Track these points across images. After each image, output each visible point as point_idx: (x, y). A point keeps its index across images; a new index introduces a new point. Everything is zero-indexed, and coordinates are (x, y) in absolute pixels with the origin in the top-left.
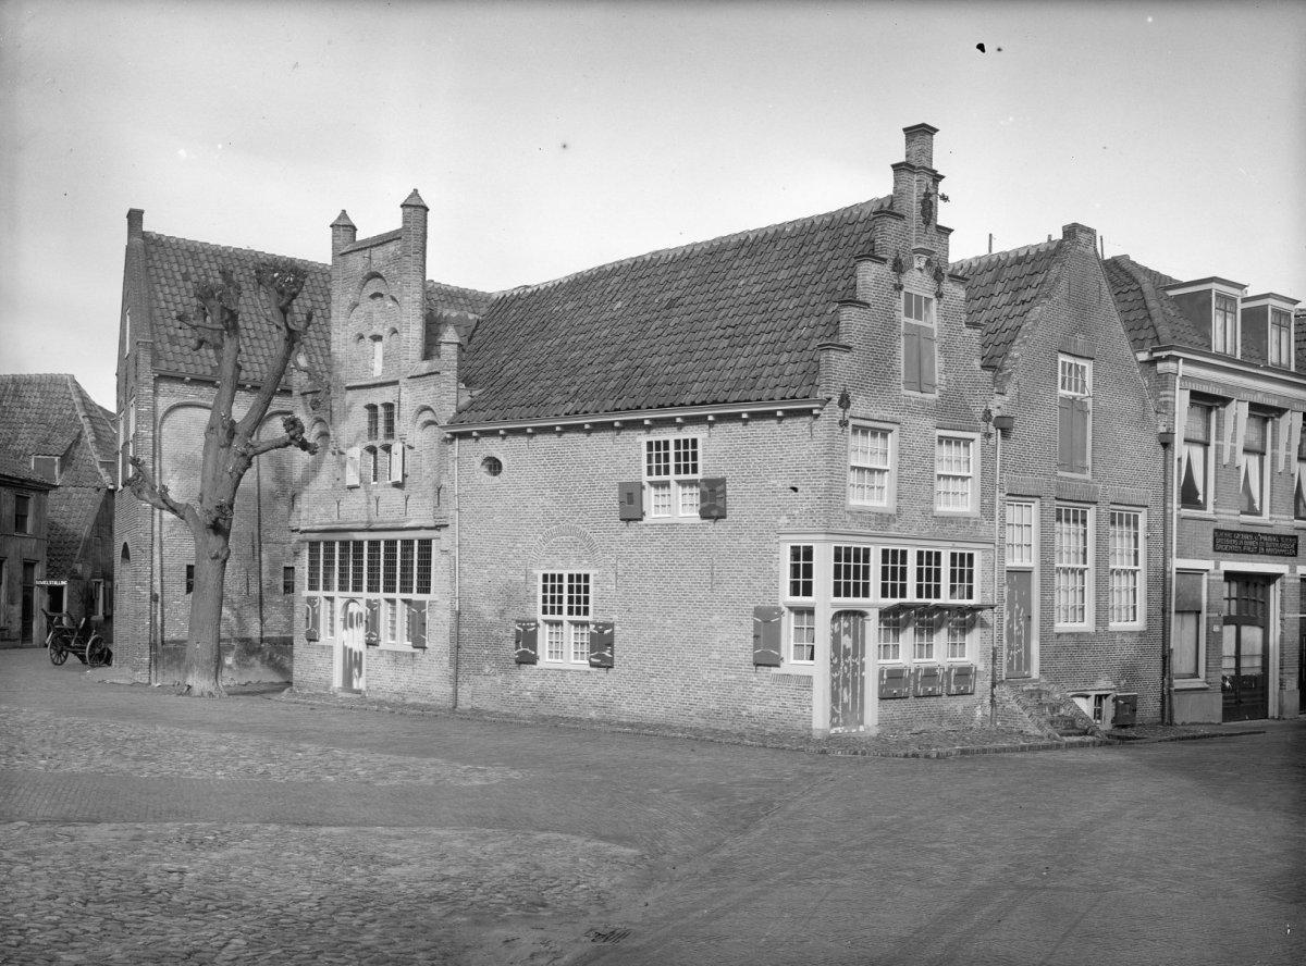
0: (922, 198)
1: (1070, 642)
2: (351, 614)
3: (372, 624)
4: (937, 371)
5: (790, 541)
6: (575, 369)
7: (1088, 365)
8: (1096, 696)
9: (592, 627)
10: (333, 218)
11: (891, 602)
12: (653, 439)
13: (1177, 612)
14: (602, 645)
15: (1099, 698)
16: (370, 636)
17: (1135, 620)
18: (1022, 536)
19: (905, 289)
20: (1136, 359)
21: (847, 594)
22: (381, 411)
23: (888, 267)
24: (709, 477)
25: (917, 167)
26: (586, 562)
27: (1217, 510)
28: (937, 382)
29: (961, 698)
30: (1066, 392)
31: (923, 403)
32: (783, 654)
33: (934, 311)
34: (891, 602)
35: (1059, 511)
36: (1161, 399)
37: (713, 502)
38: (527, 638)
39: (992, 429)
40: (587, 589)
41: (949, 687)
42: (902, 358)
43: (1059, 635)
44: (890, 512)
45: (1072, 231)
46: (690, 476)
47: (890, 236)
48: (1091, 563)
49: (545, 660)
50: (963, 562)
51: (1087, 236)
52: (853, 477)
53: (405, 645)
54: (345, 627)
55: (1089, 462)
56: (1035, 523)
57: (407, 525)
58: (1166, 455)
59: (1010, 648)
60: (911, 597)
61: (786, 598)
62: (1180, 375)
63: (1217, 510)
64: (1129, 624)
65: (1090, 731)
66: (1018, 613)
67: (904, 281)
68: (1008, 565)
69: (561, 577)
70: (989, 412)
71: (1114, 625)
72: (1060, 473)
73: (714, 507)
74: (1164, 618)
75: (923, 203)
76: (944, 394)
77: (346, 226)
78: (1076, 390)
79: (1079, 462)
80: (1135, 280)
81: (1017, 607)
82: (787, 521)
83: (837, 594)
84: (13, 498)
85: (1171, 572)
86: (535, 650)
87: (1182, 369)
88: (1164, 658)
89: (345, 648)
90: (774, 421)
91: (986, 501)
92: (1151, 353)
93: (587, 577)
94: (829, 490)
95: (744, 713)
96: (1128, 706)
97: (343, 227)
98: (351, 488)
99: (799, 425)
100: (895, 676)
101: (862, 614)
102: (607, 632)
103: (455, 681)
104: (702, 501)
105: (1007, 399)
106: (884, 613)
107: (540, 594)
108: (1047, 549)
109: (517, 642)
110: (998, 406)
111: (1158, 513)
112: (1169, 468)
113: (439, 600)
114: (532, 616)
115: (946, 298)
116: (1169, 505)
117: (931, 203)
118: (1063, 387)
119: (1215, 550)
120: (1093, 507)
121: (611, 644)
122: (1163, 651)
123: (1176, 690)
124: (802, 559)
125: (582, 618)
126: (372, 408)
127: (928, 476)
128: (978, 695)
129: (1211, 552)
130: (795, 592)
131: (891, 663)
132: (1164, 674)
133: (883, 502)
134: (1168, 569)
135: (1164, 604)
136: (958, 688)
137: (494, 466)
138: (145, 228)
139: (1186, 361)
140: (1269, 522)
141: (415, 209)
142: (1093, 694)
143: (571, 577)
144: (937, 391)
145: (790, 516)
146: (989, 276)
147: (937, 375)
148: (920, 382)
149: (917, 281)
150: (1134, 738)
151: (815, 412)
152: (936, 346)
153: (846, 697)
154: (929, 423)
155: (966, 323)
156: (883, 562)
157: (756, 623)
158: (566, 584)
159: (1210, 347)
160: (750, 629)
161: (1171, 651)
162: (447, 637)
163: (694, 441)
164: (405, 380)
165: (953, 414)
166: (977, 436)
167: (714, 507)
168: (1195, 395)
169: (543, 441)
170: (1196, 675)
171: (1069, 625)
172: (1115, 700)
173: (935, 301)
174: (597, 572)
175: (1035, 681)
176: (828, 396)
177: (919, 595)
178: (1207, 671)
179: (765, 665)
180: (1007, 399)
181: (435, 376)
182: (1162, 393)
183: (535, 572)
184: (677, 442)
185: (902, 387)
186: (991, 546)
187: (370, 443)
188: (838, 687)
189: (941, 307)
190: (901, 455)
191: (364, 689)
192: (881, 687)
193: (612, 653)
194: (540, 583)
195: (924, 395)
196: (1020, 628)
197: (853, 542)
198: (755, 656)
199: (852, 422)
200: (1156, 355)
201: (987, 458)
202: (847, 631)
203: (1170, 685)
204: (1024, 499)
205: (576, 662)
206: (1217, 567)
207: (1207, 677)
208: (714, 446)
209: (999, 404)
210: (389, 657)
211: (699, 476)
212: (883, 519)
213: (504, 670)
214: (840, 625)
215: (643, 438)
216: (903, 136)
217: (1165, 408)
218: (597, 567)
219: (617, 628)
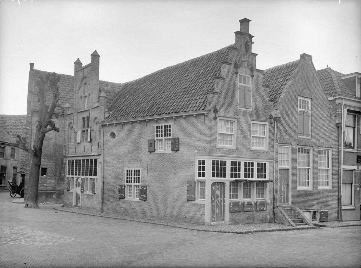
0: (245, 43)
1: (303, 193)
2: (78, 183)
3: (82, 186)
4: (251, 101)
5: (244, 160)
6: (140, 104)
7: (309, 101)
8: (313, 211)
9: (140, 187)
10: (75, 61)
11: (234, 179)
12: (158, 125)
13: (343, 183)
14: (143, 192)
15: (314, 213)
16: (81, 189)
17: (328, 186)
18: (285, 158)
19: (239, 74)
20: (327, 99)
21: (217, 176)
22: (86, 119)
23: (232, 66)
24: (174, 137)
25: (244, 35)
26: (139, 166)
27: (358, 149)
28: (252, 105)
29: (261, 212)
30: (301, 109)
31: (246, 112)
32: (196, 197)
33: (251, 82)
34: (234, 179)
35: (319, 151)
36: (337, 112)
37: (176, 146)
38: (122, 190)
39: (273, 121)
40: (139, 175)
41: (256, 208)
42: (238, 97)
43: (299, 191)
44: (234, 149)
45: (304, 56)
46: (169, 137)
47: (233, 58)
48: (330, 167)
49: (128, 198)
50: (262, 167)
51: (309, 58)
52: (219, 137)
53: (91, 193)
54: (77, 187)
55: (310, 133)
57: (91, 154)
58: (338, 131)
59: (281, 195)
60: (242, 178)
61: (197, 178)
63: (358, 149)
64: (326, 187)
65: (308, 224)
66: (284, 183)
67: (239, 71)
69: (132, 171)
70: (272, 115)
71: (320, 188)
72: (299, 136)
73: (175, 147)
74: (338, 185)
75: (246, 45)
76: (254, 109)
77: (78, 63)
78: (305, 109)
79: (306, 133)
80: (330, 75)
81: (283, 181)
82: (197, 152)
83: (213, 176)
84: (10, 149)
85: (341, 170)
86: (124, 195)
87: (344, 102)
88: (339, 198)
89: (77, 193)
90: (193, 118)
91: (271, 145)
92: (334, 97)
93: (139, 171)
94: (210, 141)
95: (184, 216)
96: (325, 215)
97: (78, 63)
98: (79, 143)
99: (201, 119)
100: (236, 204)
101: (224, 183)
102: (144, 189)
103: (102, 203)
104: (172, 145)
105: (279, 111)
106: (232, 183)
107: (126, 176)
108: (294, 161)
109: (119, 192)
110: (275, 113)
111: (335, 150)
112: (340, 135)
113: (99, 177)
114: (123, 183)
115: (255, 77)
116: (340, 147)
117: (249, 45)
118: (300, 108)
119: (357, 162)
121: (146, 193)
123: (343, 209)
124: (202, 163)
125: (138, 184)
126: (84, 118)
127: (248, 137)
128: (268, 211)
129: (356, 163)
130: (200, 176)
131: (234, 200)
132: (339, 204)
133: (232, 146)
134: (340, 169)
135: (338, 180)
136: (260, 209)
137: (113, 135)
138: (34, 69)
139: (346, 99)
140: (357, 152)
141: (95, 56)
142: (312, 211)
143: (135, 171)
144: (252, 108)
145: (199, 150)
146: (277, 73)
147: (252, 103)
149: (244, 72)
150: (326, 226)
151: (205, 114)
153: (217, 211)
154: (249, 119)
155: (263, 86)
156: (226, 167)
157: (187, 186)
158: (133, 173)
159: (355, 95)
160: (186, 188)
161: (341, 196)
162: (101, 190)
163: (170, 126)
164: (91, 109)
165: (257, 115)
166: (267, 124)
167: (175, 147)
168: (348, 111)
169: (127, 127)
170: (351, 204)
171: (303, 187)
172: (320, 213)
173: (251, 78)
174: (142, 169)
175: (290, 206)
176: (209, 109)
177: (245, 177)
178: (355, 203)
179: (191, 200)
180: (279, 111)
181: (98, 108)
182: (337, 110)
183: (125, 169)
184: (165, 126)
185: (238, 106)
187: (83, 129)
188: (214, 208)
189: (253, 80)
190: (238, 129)
191: (80, 206)
192: (230, 208)
193: (146, 196)
194: (126, 173)
195: (247, 109)
196: (284, 188)
197: (264, 161)
198: (187, 197)
199: (218, 118)
200: (335, 97)
201: (271, 131)
202: (218, 189)
203: (341, 208)
204: (285, 145)
205: (136, 198)
206: (358, 168)
207: (355, 205)
208: (176, 128)
209: (275, 113)
210: (86, 196)
211: (171, 137)
212: (231, 151)
213: (116, 201)
214: (215, 187)
215: (155, 125)
216: (239, 23)
217: (339, 116)
218: (142, 167)
219: (147, 187)
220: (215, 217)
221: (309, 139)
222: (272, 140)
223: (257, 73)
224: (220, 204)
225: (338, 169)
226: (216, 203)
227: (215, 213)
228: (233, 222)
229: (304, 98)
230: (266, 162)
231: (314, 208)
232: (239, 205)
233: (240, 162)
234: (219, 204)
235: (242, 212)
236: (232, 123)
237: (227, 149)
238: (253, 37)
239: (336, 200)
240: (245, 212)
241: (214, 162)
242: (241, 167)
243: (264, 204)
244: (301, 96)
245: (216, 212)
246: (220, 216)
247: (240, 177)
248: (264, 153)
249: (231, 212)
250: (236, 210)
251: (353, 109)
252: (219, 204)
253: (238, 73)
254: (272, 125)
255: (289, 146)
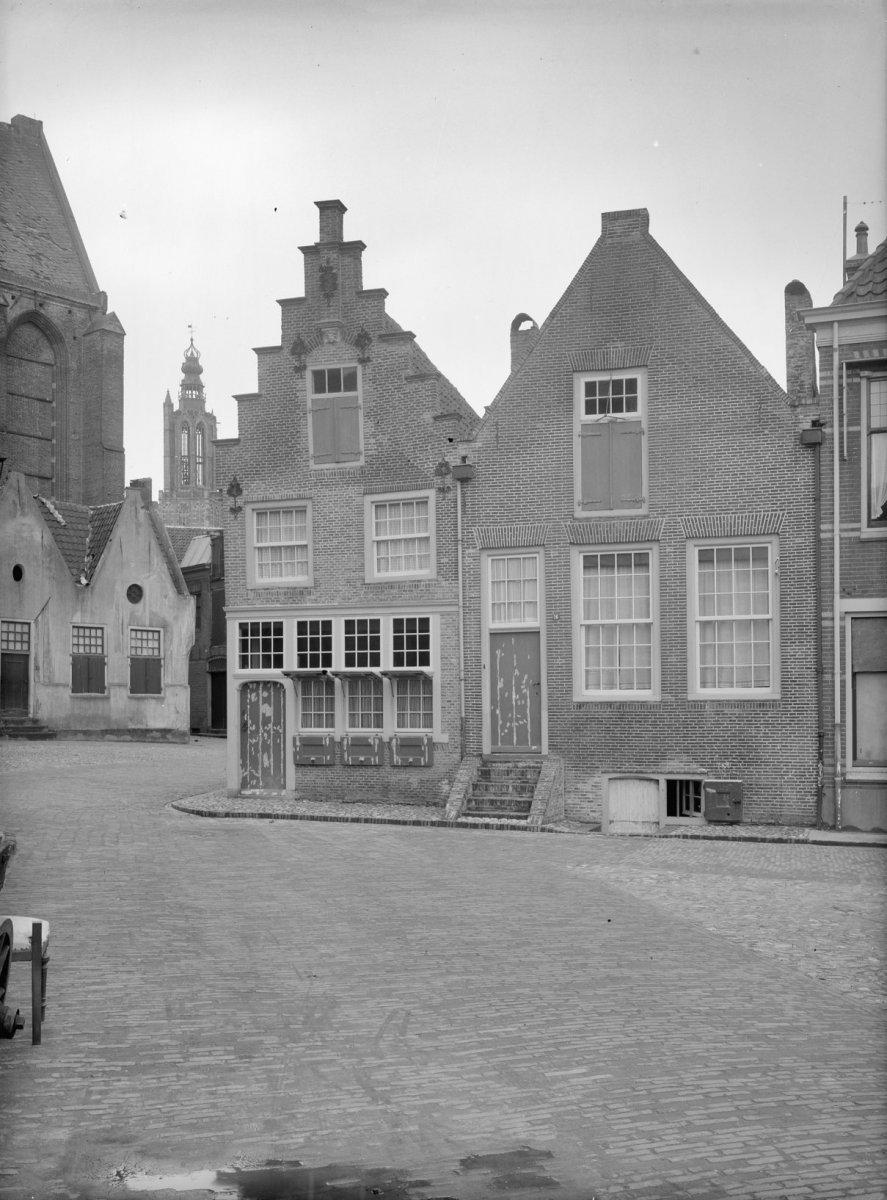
5: (343, 615)
28: (362, 447)
31: (342, 474)
39: (449, 480)
43: (580, 705)
55: (645, 493)
56: (540, 576)
58: (817, 462)
62: (836, 346)
66: (519, 679)
68: (491, 627)
81: (517, 672)
88: (820, 736)
111: (804, 540)
120: (655, 547)
122: (820, 723)
133: (300, 579)
148: (332, 451)
152: (361, 413)
154: (352, 491)
185: (311, 462)
186: (454, 609)
188: (257, 751)
189: (368, 371)
196: (523, 697)
202: (266, 700)
214: (258, 695)
220: (258, 778)
221: (645, 517)
222: (449, 542)
223: (384, 345)
224: (275, 741)
225: (819, 619)
226: (261, 739)
227: (260, 767)
228: (307, 793)
229: (609, 373)
230: (329, 619)
231: (667, 769)
232: (322, 745)
233: (427, 620)
234: (270, 742)
235: (338, 768)
236: (302, 511)
237: (282, 588)
238: (304, 250)
239: (810, 744)
240: (348, 766)
241: (244, 627)
242: (391, 634)
243: (420, 746)
244: (616, 369)
245: (263, 764)
246: (740, 779)
247: (428, 664)
248: (417, 586)
249: (298, 765)
250: (313, 761)
251: (867, 357)
252: (270, 742)
253: (304, 367)
254: (450, 495)
255: (538, 553)
